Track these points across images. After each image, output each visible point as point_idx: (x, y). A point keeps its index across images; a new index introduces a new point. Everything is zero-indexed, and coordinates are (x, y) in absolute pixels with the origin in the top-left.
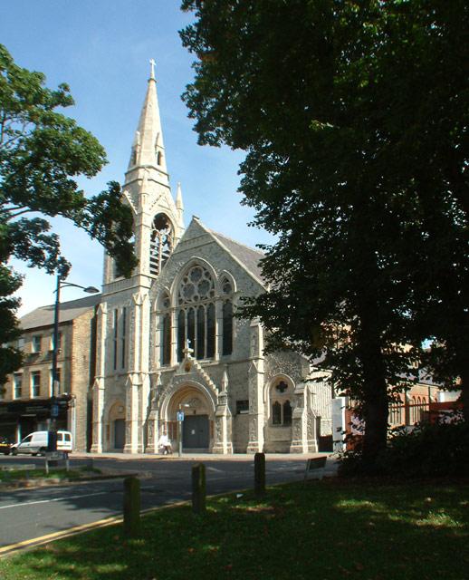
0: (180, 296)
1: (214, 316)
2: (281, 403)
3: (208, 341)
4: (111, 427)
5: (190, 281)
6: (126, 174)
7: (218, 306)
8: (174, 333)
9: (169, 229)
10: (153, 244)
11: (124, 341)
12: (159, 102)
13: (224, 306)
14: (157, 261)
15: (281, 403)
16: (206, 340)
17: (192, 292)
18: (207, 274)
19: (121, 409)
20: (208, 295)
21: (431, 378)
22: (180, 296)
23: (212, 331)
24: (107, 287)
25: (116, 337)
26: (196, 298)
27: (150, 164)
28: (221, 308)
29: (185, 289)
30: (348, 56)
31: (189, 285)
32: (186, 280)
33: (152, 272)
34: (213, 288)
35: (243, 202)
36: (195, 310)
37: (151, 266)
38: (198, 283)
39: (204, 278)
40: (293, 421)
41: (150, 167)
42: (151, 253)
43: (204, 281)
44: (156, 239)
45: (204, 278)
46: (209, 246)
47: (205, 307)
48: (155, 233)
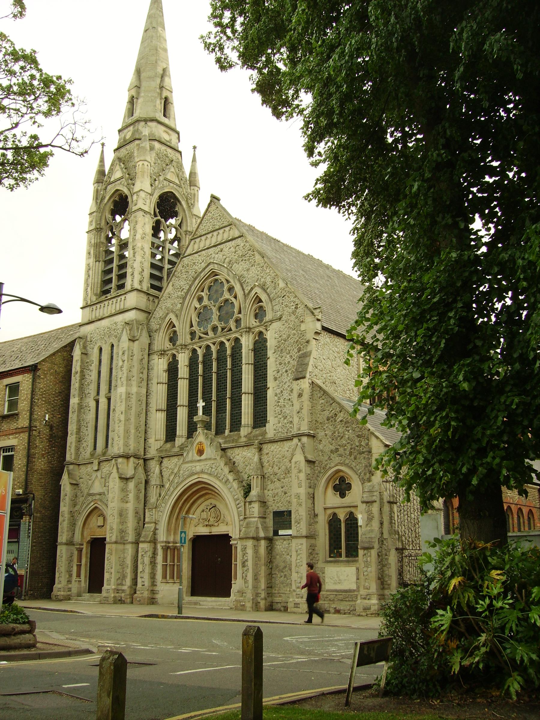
0: (192, 326)
1: (241, 361)
2: (342, 516)
3: (232, 403)
4: (84, 551)
5: (206, 302)
6: (120, 131)
7: (247, 342)
8: (183, 387)
9: (180, 218)
10: (156, 241)
11: (109, 399)
12: (266, 369)
13: (255, 343)
14: (161, 269)
15: (342, 516)
16: (228, 401)
17: (208, 320)
18: (231, 289)
19: (101, 519)
20: (232, 324)
21: (439, 160)
22: (192, 326)
23: (237, 383)
24: (87, 309)
25: (98, 393)
26: (215, 329)
27: (151, 115)
28: (251, 347)
29: (199, 314)
30: (477, 181)
31: (205, 307)
32: (200, 299)
33: (153, 286)
34: (240, 312)
35: (253, 91)
36: (214, 349)
37: (159, 289)
38: (217, 305)
39: (227, 295)
40: (361, 552)
41: (152, 120)
42: (153, 255)
43: (227, 301)
44: (162, 234)
45: (227, 295)
46: (233, 243)
47: (227, 344)
48: (158, 223)
